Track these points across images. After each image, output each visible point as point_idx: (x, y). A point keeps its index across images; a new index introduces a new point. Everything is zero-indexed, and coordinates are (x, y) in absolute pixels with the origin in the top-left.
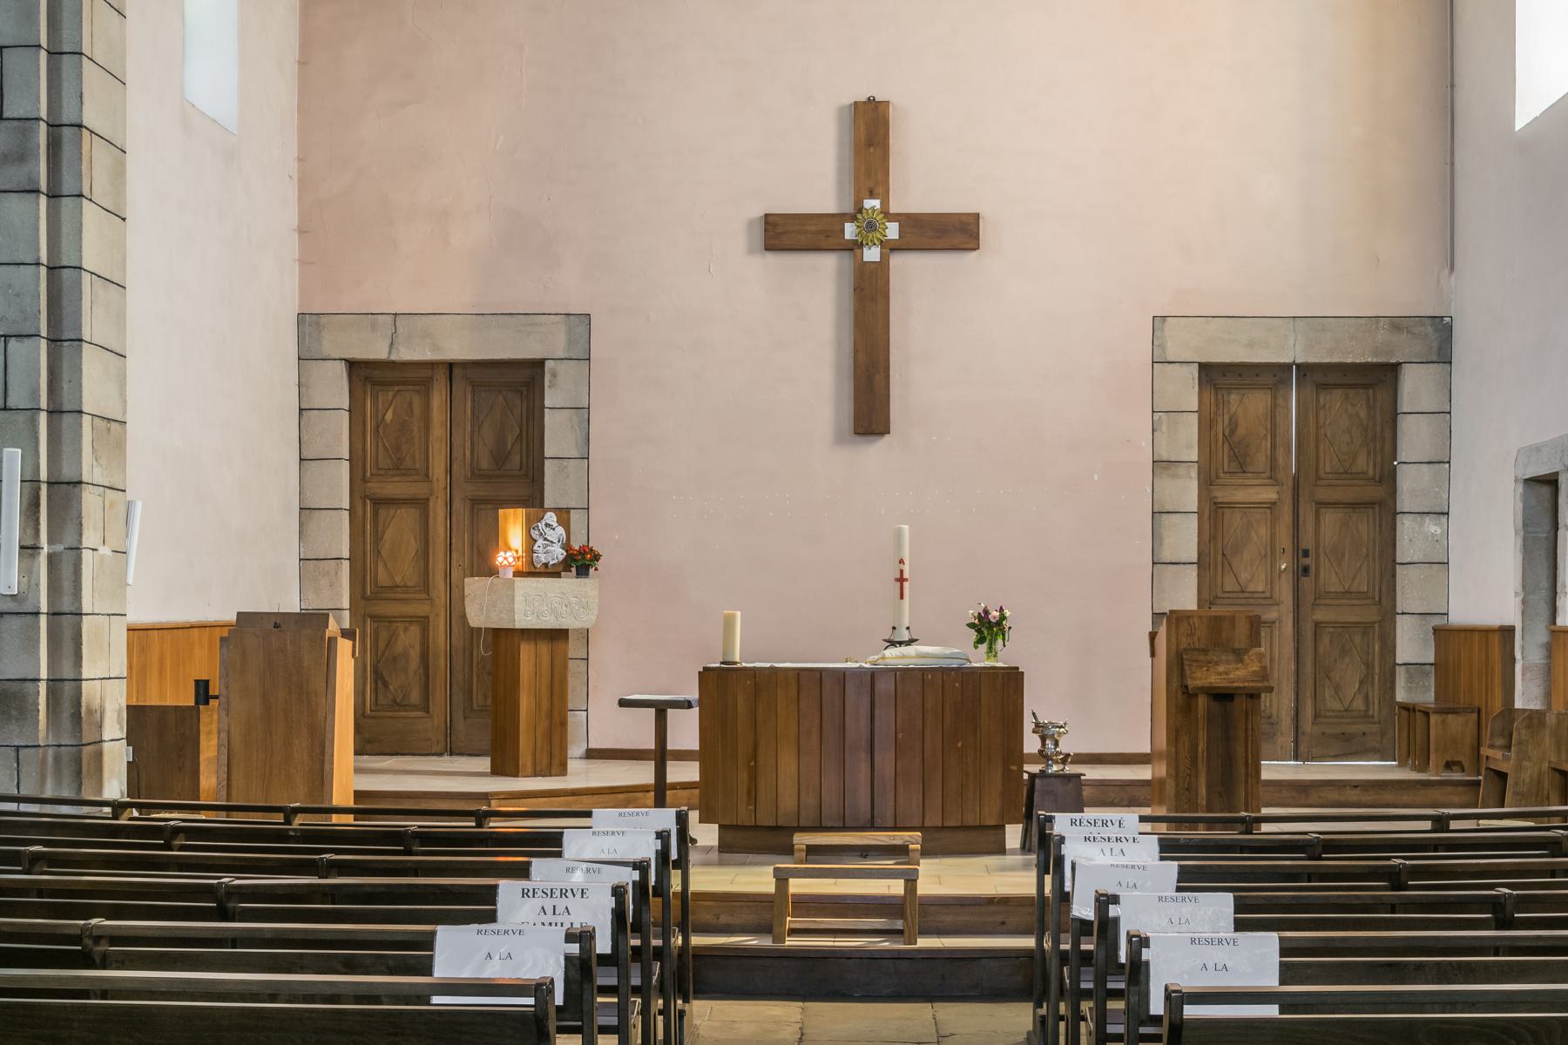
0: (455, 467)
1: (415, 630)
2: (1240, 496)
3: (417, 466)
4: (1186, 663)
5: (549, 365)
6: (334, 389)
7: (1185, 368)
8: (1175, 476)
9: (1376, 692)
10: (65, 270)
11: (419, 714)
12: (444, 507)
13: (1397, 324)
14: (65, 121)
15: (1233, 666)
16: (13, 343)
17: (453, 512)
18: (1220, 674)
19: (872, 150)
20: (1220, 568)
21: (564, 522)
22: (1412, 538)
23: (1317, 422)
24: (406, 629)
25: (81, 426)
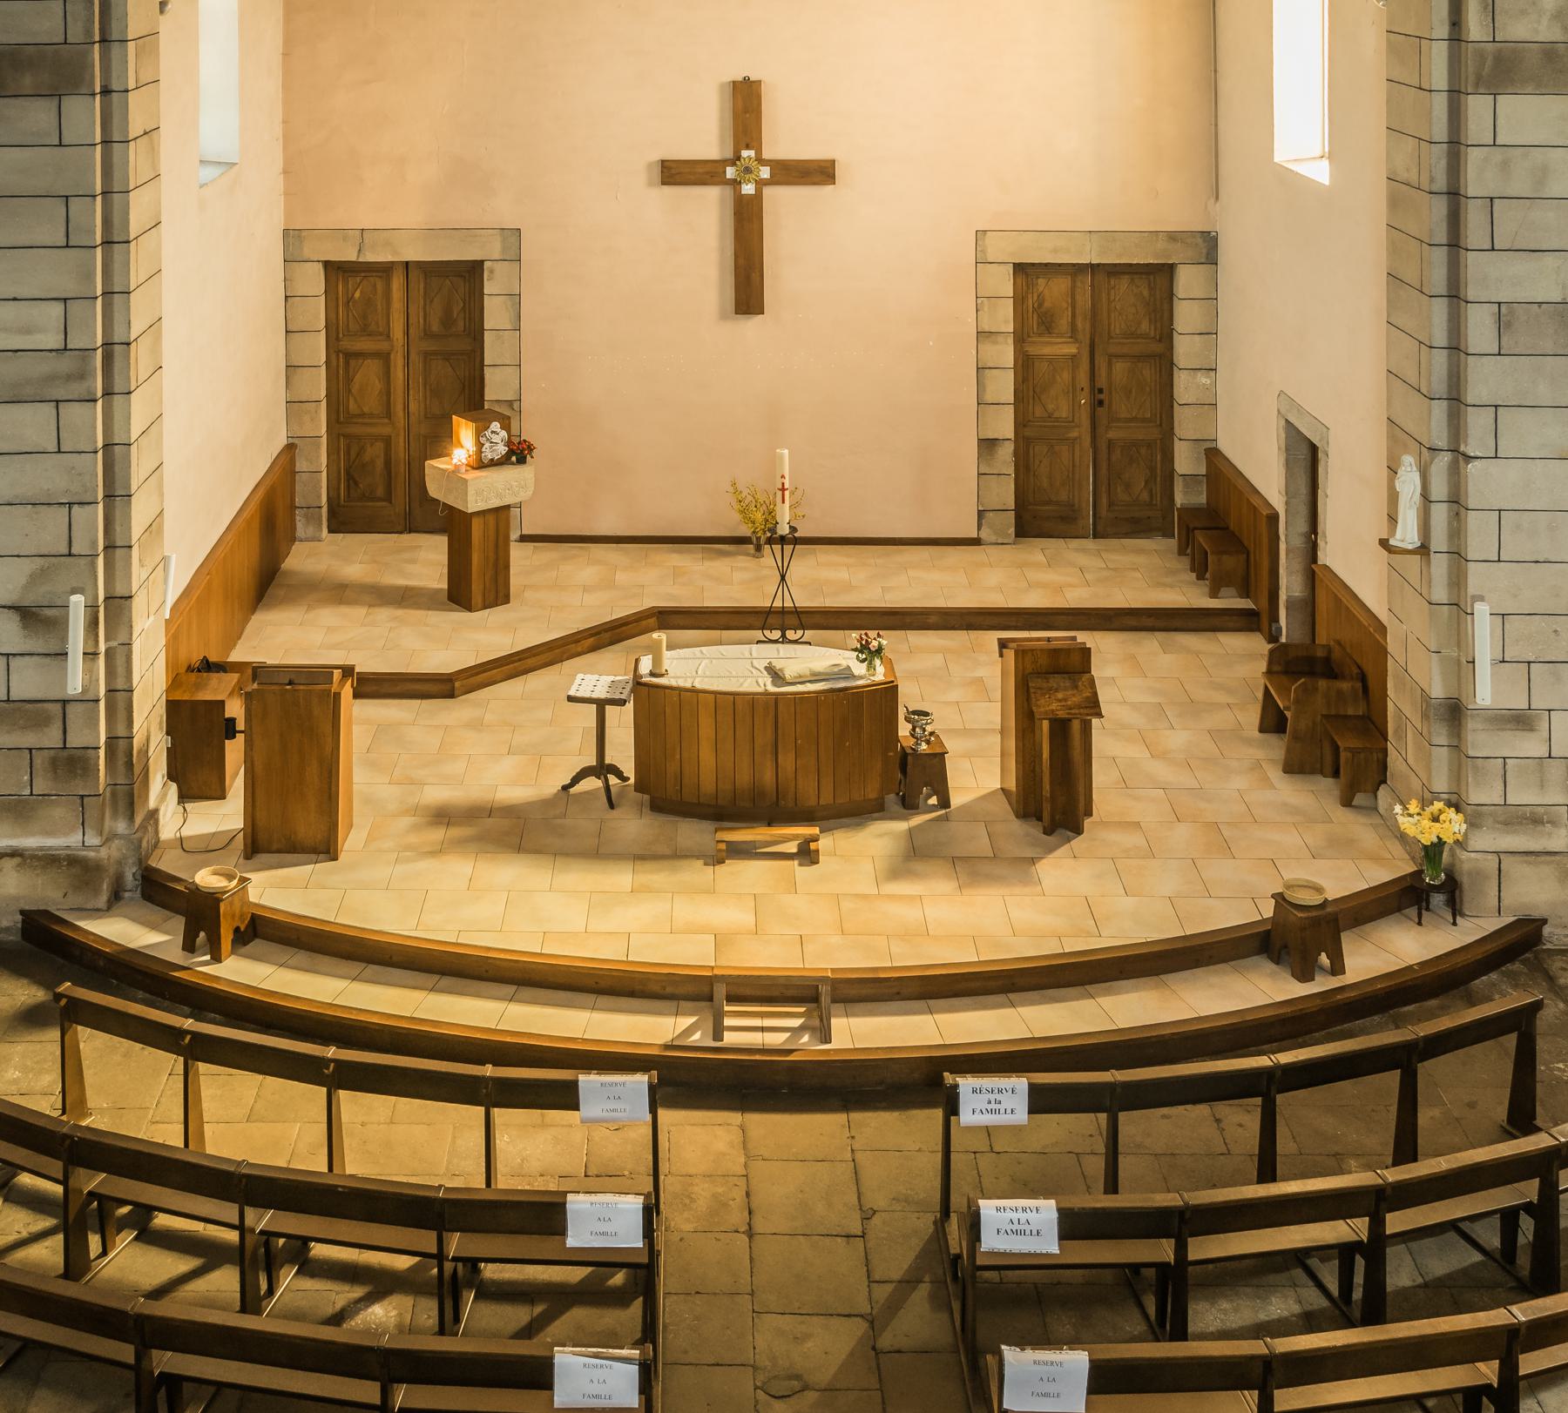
0: (411, 331)
1: (380, 446)
2: (1047, 350)
3: (381, 329)
4: (1032, 690)
5: (487, 264)
6: (313, 281)
7: (1002, 267)
8: (995, 343)
9: (1158, 489)
10: (116, 446)
11: (384, 504)
12: (402, 360)
13: (1173, 237)
14: (116, 340)
15: (1070, 692)
16: (75, 508)
17: (410, 361)
18: (1060, 701)
19: (748, 115)
20: (1031, 401)
21: (506, 427)
22: (1185, 387)
23: (1109, 299)
24: (372, 445)
25: (131, 557)
